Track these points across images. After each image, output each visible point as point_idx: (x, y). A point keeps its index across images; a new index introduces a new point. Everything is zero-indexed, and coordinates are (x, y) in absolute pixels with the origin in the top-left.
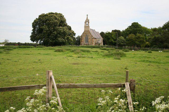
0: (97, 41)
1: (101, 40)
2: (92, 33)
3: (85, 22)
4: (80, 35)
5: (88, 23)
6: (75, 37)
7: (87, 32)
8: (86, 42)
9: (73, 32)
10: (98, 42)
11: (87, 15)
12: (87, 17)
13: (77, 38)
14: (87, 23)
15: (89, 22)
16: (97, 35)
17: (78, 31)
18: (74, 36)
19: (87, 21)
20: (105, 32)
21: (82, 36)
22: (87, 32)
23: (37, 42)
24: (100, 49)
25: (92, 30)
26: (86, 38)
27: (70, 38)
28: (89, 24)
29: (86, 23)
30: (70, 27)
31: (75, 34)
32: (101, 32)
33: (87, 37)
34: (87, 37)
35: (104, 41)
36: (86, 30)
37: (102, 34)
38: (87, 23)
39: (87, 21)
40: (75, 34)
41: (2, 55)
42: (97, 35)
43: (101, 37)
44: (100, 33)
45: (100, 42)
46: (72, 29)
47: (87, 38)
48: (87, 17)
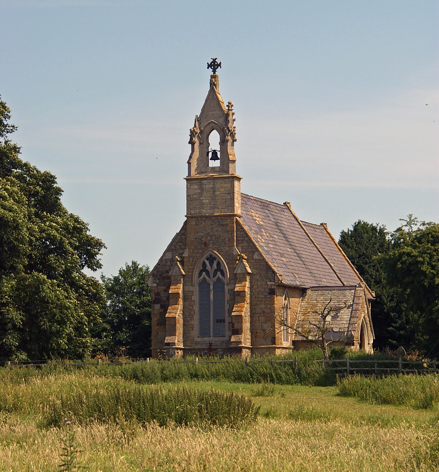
0: (315, 319)
1: (351, 313)
2: (260, 241)
3: (198, 136)
4: (149, 261)
5: (223, 142)
6: (95, 284)
7: (214, 232)
8: (204, 333)
9: (76, 228)
10: (324, 331)
11: (214, 65)
12: (213, 85)
13: (116, 287)
14: (214, 139)
15: (227, 136)
16: (309, 252)
17: (130, 226)
18: (87, 271)
19: (215, 118)
20: (390, 223)
21: (164, 272)
22: (214, 232)
23: (403, 311)
24: (344, 393)
25: (265, 205)
26: (204, 284)
27: (52, 290)
28: (237, 151)
29: (204, 143)
30: (48, 180)
31: (99, 244)
32: (349, 227)
33: (211, 281)
34: (211, 281)
35: (380, 316)
36: (206, 212)
37: (361, 243)
38: (214, 139)
39: (215, 118)
40: (89, 249)
41: (8, 371)
42: (309, 252)
43: (351, 276)
44: (344, 235)
45: (341, 323)
46: (65, 201)
47: (219, 284)
48: (213, 85)
